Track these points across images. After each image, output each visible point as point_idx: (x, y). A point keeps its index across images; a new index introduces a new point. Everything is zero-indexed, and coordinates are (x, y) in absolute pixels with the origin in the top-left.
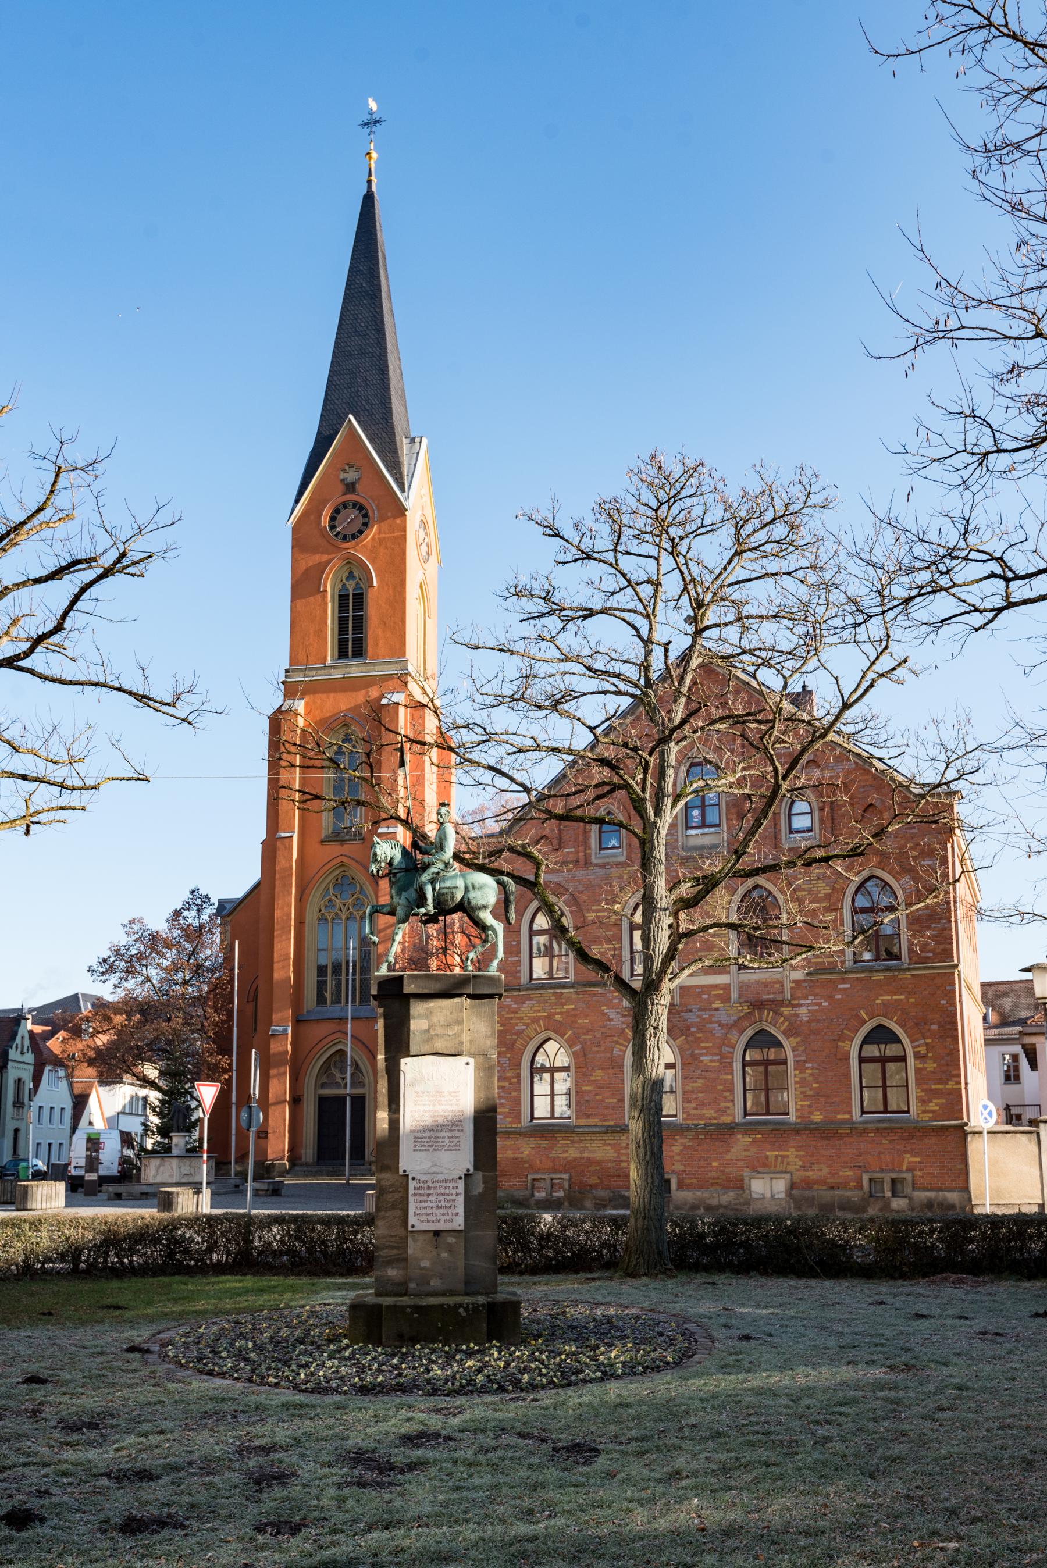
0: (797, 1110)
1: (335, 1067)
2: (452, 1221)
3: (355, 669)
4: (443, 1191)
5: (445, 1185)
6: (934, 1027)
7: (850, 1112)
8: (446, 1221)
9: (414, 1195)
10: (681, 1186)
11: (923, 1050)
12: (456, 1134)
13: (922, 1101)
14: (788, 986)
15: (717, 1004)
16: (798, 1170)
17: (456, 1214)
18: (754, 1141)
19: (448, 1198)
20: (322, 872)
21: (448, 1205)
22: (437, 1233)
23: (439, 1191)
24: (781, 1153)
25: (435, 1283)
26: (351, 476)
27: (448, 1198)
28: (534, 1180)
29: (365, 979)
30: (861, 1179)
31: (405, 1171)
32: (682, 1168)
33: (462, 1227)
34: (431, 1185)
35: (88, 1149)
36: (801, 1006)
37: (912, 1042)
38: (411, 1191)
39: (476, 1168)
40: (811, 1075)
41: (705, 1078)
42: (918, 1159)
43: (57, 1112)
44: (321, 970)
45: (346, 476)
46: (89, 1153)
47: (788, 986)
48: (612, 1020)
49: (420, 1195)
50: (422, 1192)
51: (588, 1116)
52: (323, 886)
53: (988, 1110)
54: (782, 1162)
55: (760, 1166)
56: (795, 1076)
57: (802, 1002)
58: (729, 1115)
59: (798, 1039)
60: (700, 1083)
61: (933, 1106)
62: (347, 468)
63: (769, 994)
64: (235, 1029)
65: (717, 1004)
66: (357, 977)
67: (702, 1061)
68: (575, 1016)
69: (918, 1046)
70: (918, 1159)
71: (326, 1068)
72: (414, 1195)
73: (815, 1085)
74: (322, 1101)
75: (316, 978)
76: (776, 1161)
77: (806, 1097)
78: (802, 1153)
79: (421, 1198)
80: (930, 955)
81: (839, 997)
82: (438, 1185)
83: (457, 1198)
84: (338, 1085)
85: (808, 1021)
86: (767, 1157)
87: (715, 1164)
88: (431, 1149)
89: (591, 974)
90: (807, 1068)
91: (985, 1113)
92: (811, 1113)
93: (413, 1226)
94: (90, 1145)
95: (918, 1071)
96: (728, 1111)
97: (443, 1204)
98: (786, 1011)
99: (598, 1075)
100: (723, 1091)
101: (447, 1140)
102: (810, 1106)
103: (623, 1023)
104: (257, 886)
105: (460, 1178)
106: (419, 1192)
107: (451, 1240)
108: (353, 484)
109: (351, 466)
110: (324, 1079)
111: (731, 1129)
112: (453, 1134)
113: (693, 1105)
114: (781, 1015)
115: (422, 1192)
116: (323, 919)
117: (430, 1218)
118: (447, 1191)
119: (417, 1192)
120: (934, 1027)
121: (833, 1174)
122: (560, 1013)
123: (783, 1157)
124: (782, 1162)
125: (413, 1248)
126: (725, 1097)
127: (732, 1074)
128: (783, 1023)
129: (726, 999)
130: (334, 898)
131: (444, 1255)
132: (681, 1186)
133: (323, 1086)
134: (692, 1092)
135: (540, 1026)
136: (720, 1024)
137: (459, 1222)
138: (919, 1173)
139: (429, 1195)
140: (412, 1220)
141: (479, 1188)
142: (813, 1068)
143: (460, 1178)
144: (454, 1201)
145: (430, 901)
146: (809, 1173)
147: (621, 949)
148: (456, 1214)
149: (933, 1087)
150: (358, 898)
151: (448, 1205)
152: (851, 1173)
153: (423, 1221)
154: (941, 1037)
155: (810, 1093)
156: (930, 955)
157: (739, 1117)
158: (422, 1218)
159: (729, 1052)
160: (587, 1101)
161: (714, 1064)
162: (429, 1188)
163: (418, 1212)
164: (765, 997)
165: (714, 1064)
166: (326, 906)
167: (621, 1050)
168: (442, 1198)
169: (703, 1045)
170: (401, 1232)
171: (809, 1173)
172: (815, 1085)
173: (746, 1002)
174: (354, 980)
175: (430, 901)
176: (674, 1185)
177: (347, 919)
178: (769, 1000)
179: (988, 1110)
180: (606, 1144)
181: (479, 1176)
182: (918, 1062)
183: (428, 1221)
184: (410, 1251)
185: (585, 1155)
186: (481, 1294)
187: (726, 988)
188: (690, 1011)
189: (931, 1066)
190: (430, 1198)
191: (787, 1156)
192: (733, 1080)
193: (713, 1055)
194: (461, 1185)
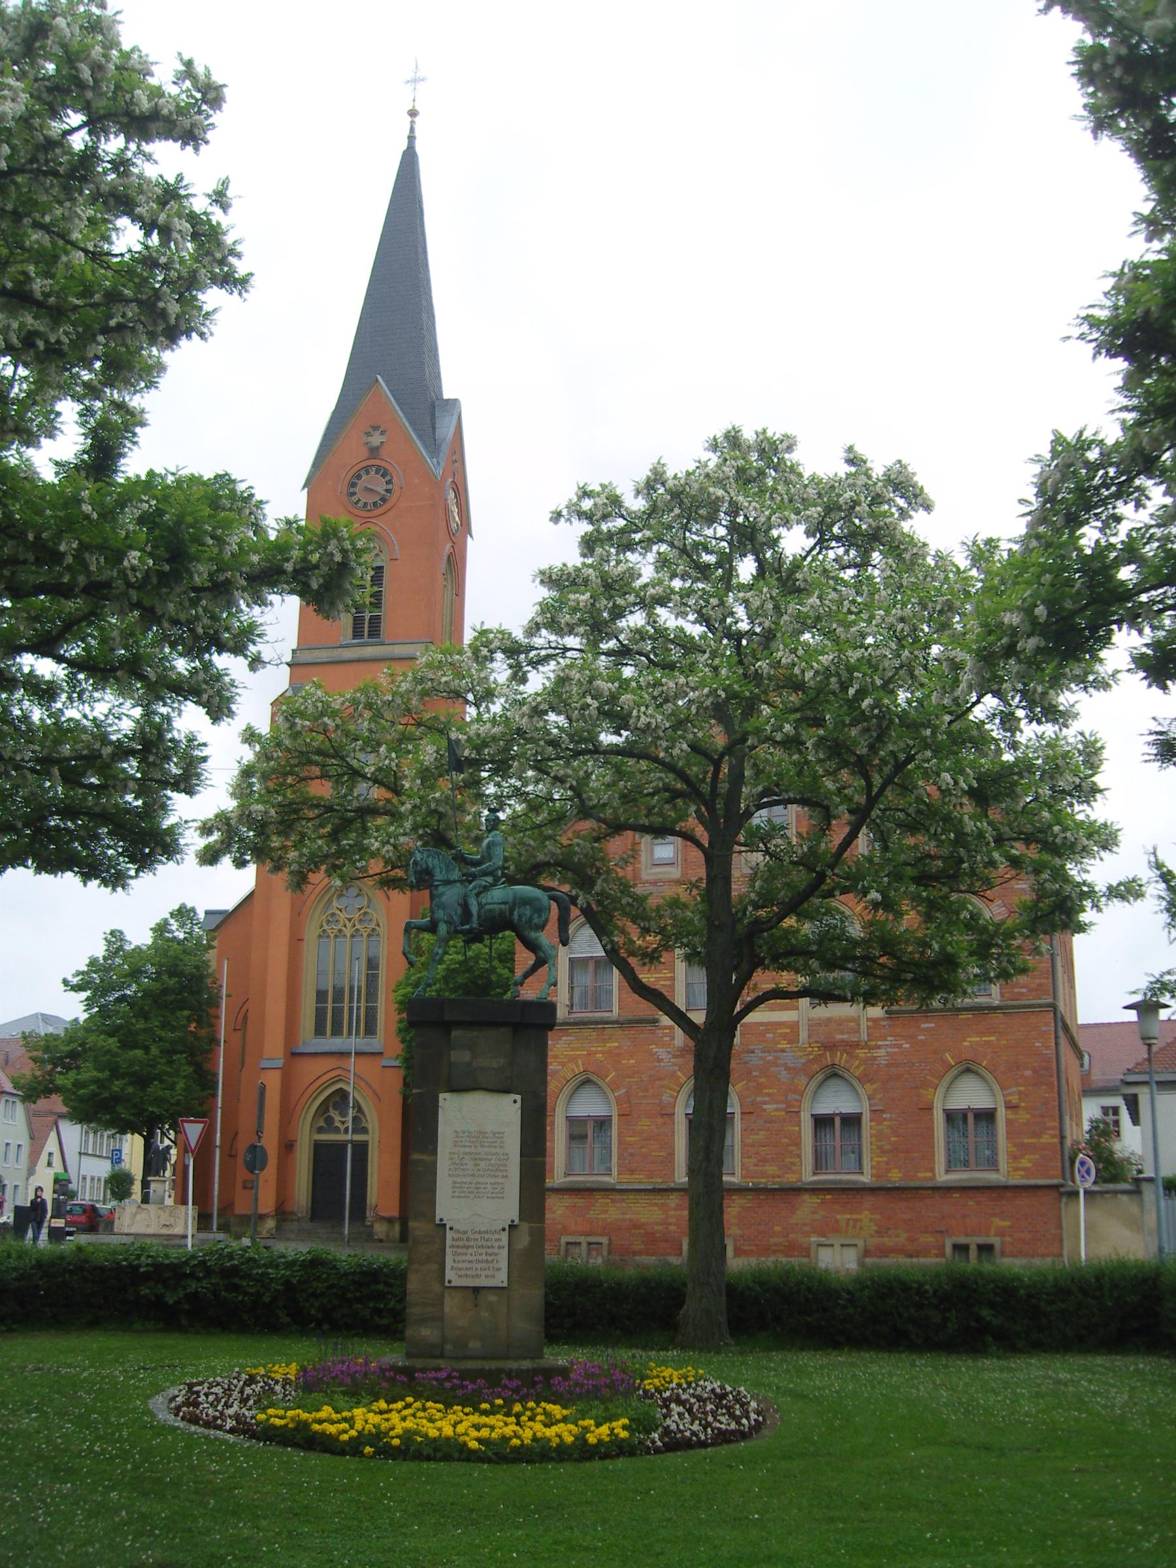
0: (872, 1167)
1: (335, 1108)
2: (494, 1277)
3: (370, 651)
4: (484, 1243)
5: (486, 1236)
6: (1028, 1073)
7: (932, 1170)
8: (487, 1276)
9: (452, 1246)
10: (738, 1252)
11: (1015, 1099)
12: (500, 1180)
13: (1014, 1158)
14: (864, 1024)
15: (783, 1045)
16: (872, 1236)
17: (499, 1269)
18: (824, 1202)
19: (490, 1251)
20: (310, 1091)
21: (490, 1258)
22: (476, 1290)
23: (480, 1243)
24: (854, 1216)
25: (475, 1345)
26: (376, 440)
27: (490, 1251)
28: (568, 1243)
29: (371, 1008)
30: (944, 1246)
31: (441, 1220)
32: (739, 1232)
33: (505, 1284)
34: (472, 1236)
35: (55, 1192)
36: (879, 1047)
37: (1002, 1089)
38: (449, 1242)
39: (521, 1218)
40: (889, 1127)
41: (768, 1130)
42: (1007, 1223)
43: (13, 1148)
44: (321, 995)
45: (370, 439)
46: (56, 1196)
47: (864, 1024)
48: (661, 1061)
49: (458, 1247)
50: (461, 1243)
51: (632, 1172)
52: (327, 898)
53: (1086, 1167)
54: (854, 1227)
55: (827, 1228)
56: (871, 1128)
57: (880, 1043)
58: (794, 1172)
59: (874, 1086)
60: (762, 1135)
61: (1025, 1163)
62: (370, 430)
63: (843, 1033)
64: (216, 1193)
65: (783, 1045)
66: (363, 1004)
67: (765, 1110)
68: (619, 1055)
69: (1010, 1094)
70: (1007, 1223)
71: (324, 1108)
72: (452, 1246)
73: (893, 1139)
74: (318, 1147)
75: (315, 1005)
76: (847, 1225)
77: (884, 1152)
78: (877, 1216)
79: (459, 1251)
80: (1024, 990)
81: (923, 1037)
82: (478, 1236)
83: (501, 1251)
84: (337, 1130)
85: (887, 1065)
86: (837, 1221)
87: (777, 1228)
88: (472, 1196)
89: (645, 1008)
90: (885, 1119)
91: (1083, 1170)
92: (889, 1170)
93: (450, 1282)
94: (57, 1187)
95: (1009, 1122)
96: (794, 1168)
97: (484, 1257)
98: (861, 1053)
99: (644, 1124)
100: (789, 1145)
101: (489, 1186)
102: (887, 1163)
103: (675, 1064)
104: (249, 898)
105: (504, 1230)
106: (458, 1243)
107: (492, 1298)
108: (377, 448)
109: (376, 428)
110: (322, 1123)
111: (797, 1190)
112: (497, 1180)
113: (754, 1160)
114: (857, 1057)
115: (461, 1243)
116: (323, 935)
117: (469, 1272)
118: (489, 1244)
119: (455, 1243)
120: (1028, 1073)
121: (911, 1240)
122: (602, 1052)
123: (856, 1221)
124: (854, 1227)
125: (450, 1305)
126: (791, 1152)
127: (799, 1125)
128: (858, 1067)
129: (793, 1037)
130: (338, 912)
131: (485, 1314)
132: (738, 1252)
133: (320, 1130)
134: (753, 1146)
135: (577, 1066)
136: (787, 1068)
137: (501, 1278)
138: (1008, 1239)
139: (468, 1247)
140: (449, 1274)
141: (524, 1241)
142: (891, 1120)
143: (504, 1230)
144: (496, 1254)
145: (475, 919)
146: (886, 1240)
147: (673, 979)
148: (499, 1269)
149: (1026, 1141)
150: (366, 913)
151: (490, 1258)
152: (931, 1239)
153: (460, 1276)
154: (1035, 1085)
155: (887, 1147)
156: (1024, 990)
157: (808, 1176)
158: (460, 1273)
159: (797, 1100)
160: (632, 1155)
161: (777, 1113)
162: (468, 1239)
163: (456, 1265)
164: (838, 1037)
165: (777, 1113)
166: (328, 922)
167: (671, 1096)
168: (483, 1251)
169: (766, 1091)
170: (437, 1287)
171: (886, 1240)
172: (893, 1139)
173: (816, 1042)
174: (358, 1008)
175: (475, 919)
176: (730, 1252)
177: (353, 936)
178: (842, 1041)
179: (1086, 1167)
180: (651, 1205)
181: (525, 1227)
182: (1009, 1112)
183: (467, 1276)
184: (447, 1309)
185: (628, 1217)
186: (525, 1358)
187: (794, 1026)
188: (753, 1052)
189: (1023, 1116)
190: (470, 1251)
191: (860, 1220)
192: (799, 1133)
193: (777, 1103)
194: (505, 1237)
